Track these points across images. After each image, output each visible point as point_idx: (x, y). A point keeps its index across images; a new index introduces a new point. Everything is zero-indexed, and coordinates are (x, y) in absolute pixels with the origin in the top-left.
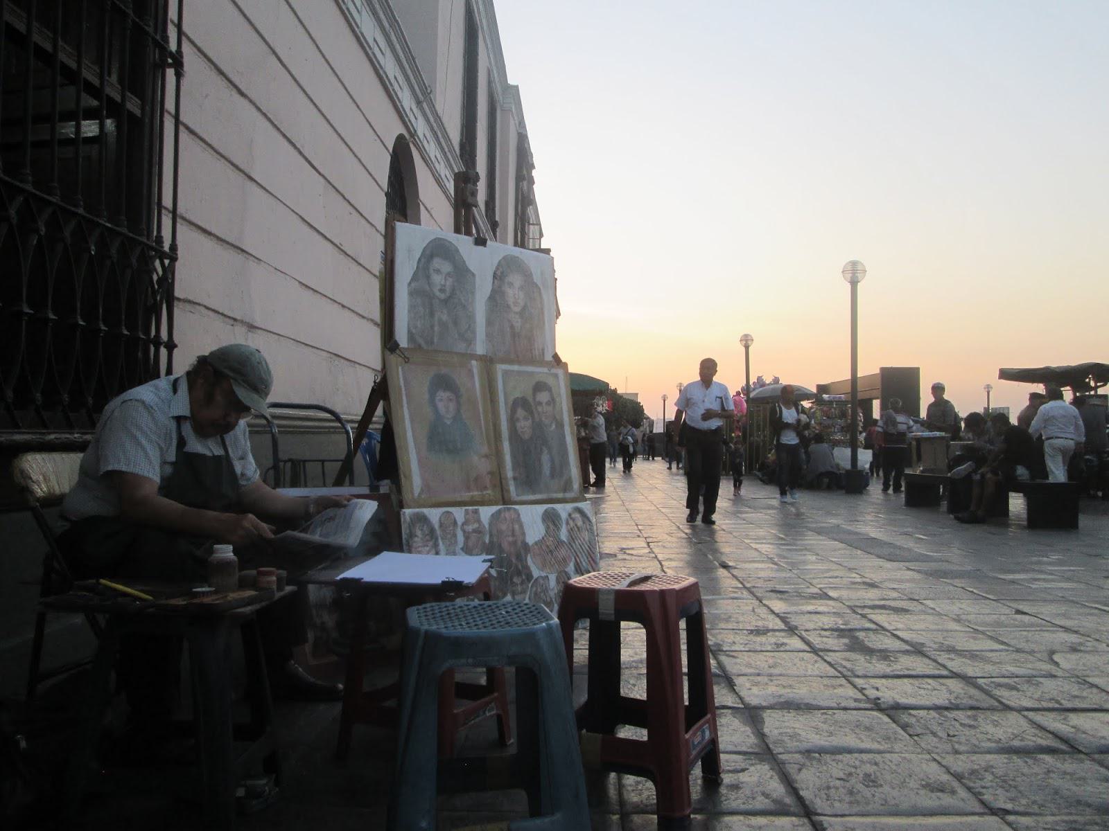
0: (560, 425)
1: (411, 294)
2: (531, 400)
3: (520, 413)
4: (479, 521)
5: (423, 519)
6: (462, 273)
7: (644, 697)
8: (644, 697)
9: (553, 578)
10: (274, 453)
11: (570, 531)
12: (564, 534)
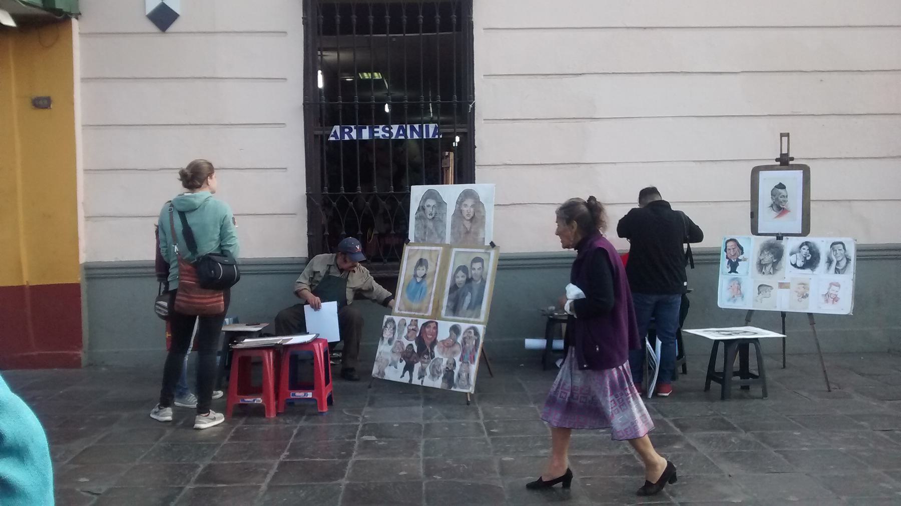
0: (484, 282)
1: (416, 219)
2: (469, 267)
3: (461, 273)
4: (416, 325)
5: (393, 321)
6: (441, 204)
7: (335, 303)
8: (335, 303)
9: (445, 360)
10: (809, 179)
11: (464, 339)
12: (460, 340)
